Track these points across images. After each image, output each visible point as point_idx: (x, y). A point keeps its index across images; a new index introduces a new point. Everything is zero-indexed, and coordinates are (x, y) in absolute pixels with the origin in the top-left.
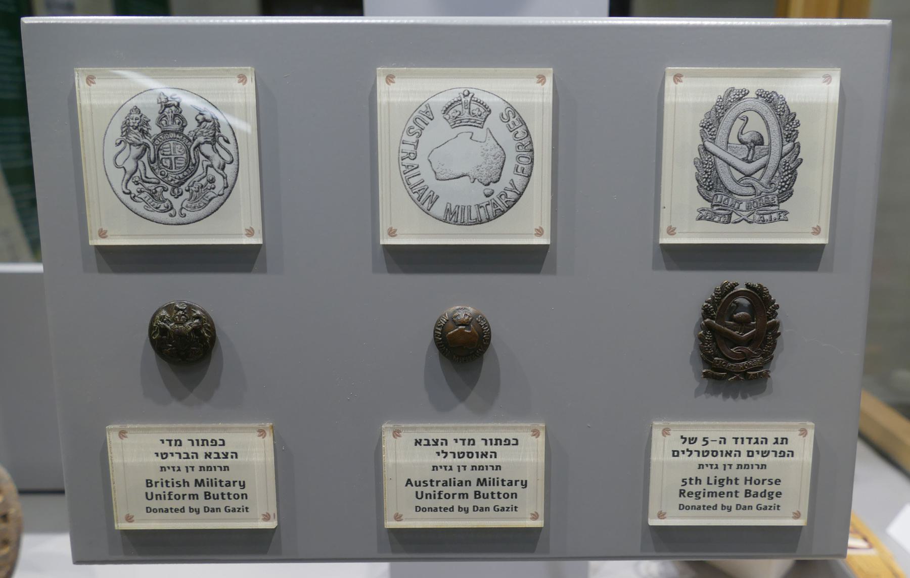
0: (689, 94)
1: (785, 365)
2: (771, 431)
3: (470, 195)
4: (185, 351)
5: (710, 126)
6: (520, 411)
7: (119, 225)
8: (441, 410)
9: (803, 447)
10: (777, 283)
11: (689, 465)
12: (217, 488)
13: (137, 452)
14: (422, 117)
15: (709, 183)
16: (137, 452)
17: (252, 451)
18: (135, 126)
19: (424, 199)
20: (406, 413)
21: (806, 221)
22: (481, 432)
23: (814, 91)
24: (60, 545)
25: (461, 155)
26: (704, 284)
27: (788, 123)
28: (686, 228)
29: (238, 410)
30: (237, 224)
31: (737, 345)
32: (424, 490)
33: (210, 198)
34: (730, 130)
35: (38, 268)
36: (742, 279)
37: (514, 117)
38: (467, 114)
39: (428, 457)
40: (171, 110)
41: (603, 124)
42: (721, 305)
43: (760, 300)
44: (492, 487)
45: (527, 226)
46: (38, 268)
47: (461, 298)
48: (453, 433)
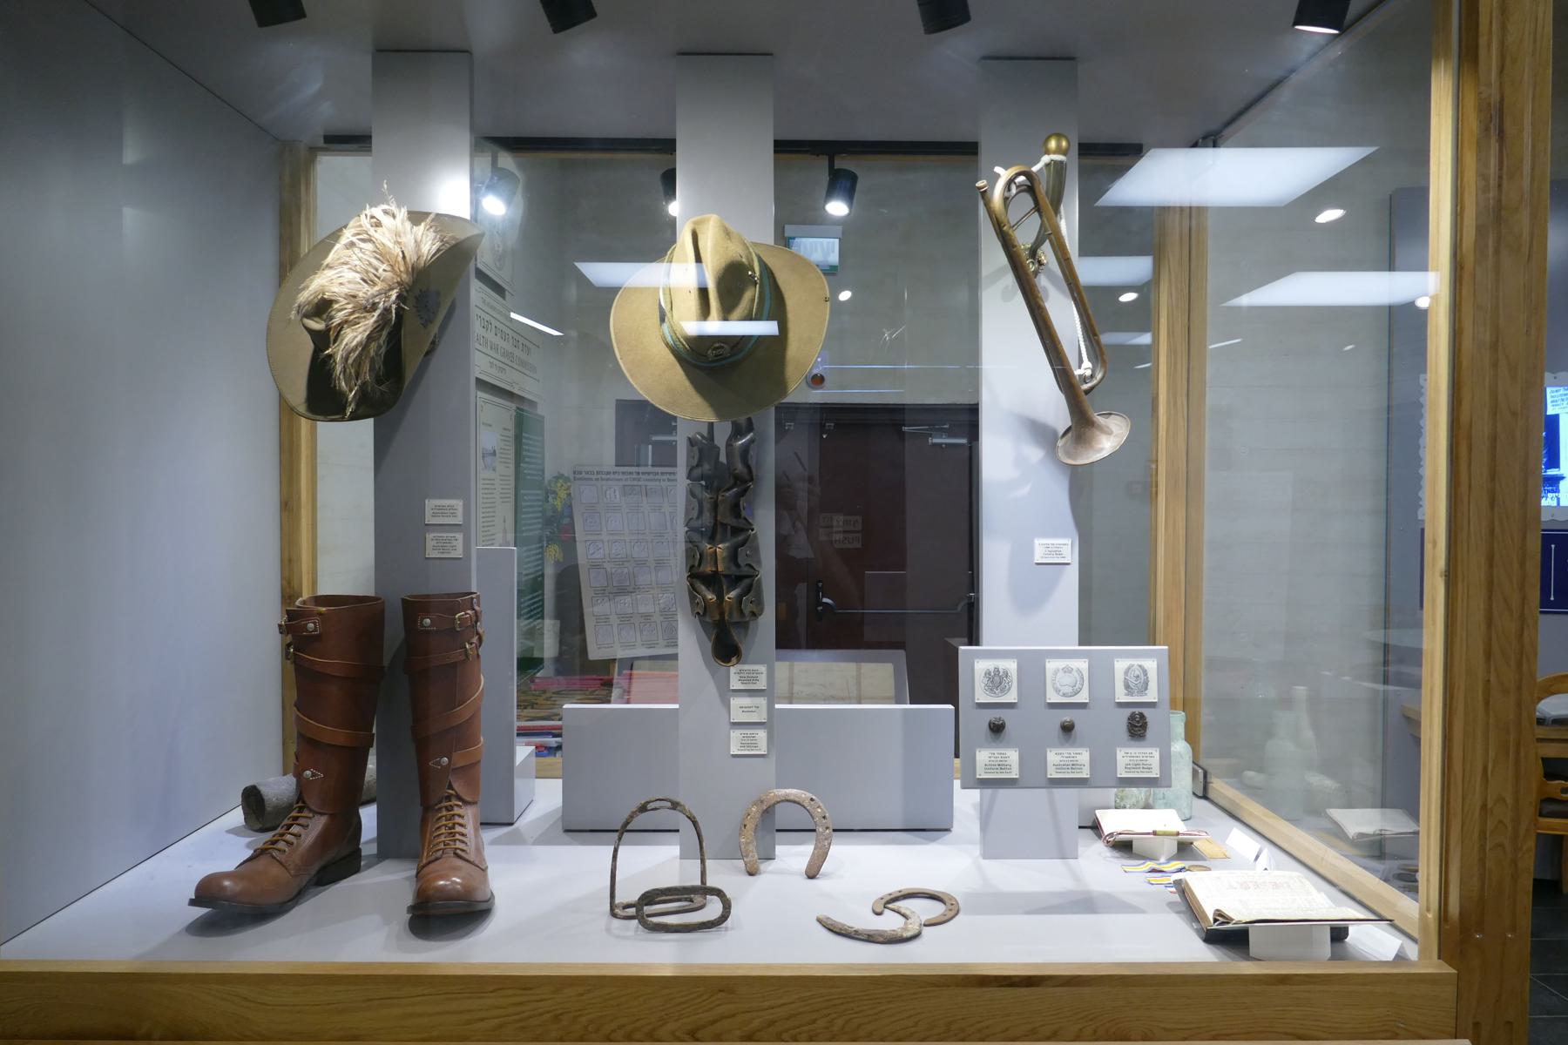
0: (1120, 665)
1: (1150, 733)
2: (1148, 750)
3: (1069, 690)
4: (997, 729)
5: (1126, 673)
6: (1082, 746)
7: (982, 697)
8: (1062, 745)
9: (1156, 753)
10: (1146, 712)
11: (1127, 760)
12: (1003, 766)
13: (983, 756)
14: (1056, 672)
15: (1127, 686)
16: (983, 756)
17: (1013, 756)
18: (988, 673)
19: (1057, 691)
20: (1053, 746)
21: (1151, 696)
22: (1072, 751)
23: (1151, 665)
24: (1548, 501)
25: (1066, 680)
26: (1128, 712)
27: (1145, 672)
28: (1121, 696)
29: (1009, 745)
30: (1011, 697)
31: (1137, 728)
32: (1058, 767)
33: (1004, 691)
34: (1131, 674)
35: (676, 706)
36: (1137, 710)
37: (1079, 671)
38: (1068, 670)
39: (1059, 758)
40: (997, 670)
41: (1100, 675)
42: (1132, 717)
43: (1142, 716)
44: (1075, 766)
45: (1083, 697)
46: (676, 706)
47: (1066, 716)
48: (1065, 751)
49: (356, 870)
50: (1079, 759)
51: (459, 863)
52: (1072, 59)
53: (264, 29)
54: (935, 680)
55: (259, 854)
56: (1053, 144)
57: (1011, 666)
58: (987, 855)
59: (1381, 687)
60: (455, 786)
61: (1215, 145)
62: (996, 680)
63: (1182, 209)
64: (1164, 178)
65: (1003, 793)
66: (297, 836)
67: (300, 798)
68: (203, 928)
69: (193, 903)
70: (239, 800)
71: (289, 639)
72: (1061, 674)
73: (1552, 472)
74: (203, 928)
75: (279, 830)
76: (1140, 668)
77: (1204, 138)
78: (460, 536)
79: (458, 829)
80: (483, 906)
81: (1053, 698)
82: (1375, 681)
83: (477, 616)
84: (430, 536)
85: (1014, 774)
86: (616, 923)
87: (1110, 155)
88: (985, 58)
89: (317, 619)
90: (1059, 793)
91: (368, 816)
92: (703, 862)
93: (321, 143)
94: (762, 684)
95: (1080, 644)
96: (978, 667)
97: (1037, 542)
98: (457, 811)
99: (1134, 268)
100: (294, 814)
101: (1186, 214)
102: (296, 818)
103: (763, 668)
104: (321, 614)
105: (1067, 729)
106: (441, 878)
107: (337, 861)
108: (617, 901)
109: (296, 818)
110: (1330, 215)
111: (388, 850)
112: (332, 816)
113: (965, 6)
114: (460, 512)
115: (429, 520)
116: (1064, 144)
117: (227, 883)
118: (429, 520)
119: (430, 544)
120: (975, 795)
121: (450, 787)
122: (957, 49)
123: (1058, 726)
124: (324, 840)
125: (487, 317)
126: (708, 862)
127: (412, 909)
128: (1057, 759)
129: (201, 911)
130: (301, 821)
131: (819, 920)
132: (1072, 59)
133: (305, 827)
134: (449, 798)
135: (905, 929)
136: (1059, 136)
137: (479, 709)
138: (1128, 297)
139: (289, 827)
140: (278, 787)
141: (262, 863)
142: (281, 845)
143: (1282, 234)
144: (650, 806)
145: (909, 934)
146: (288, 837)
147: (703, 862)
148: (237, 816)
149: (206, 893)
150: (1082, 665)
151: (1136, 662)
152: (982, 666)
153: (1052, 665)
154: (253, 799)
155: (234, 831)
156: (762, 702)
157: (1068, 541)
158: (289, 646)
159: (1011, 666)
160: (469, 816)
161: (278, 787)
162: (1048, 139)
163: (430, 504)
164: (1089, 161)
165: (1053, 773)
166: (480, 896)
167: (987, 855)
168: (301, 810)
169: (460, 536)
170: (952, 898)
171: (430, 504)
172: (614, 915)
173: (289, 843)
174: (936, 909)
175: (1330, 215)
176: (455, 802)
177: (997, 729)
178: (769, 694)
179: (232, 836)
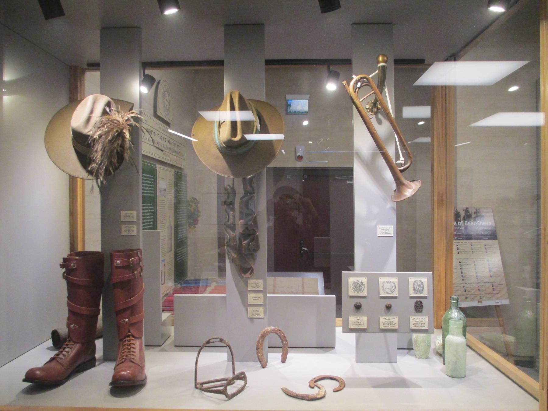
0: (412, 280)
2: (423, 317)
3: (389, 291)
4: (358, 307)
5: (414, 283)
7: (351, 293)
10: (422, 300)
12: (360, 323)
13: (352, 319)
14: (384, 282)
15: (414, 289)
16: (382, 319)
18: (354, 283)
19: (384, 291)
21: (425, 294)
22: (391, 317)
23: (425, 280)
25: (388, 286)
26: (415, 300)
27: (422, 283)
28: (412, 294)
30: (364, 293)
31: (419, 307)
32: (385, 324)
33: (361, 291)
36: (419, 300)
38: (389, 282)
39: (385, 320)
40: (358, 281)
41: (403, 285)
42: (417, 302)
43: (421, 302)
44: (391, 323)
45: (395, 294)
47: (388, 302)
49: (94, 366)
50: (393, 320)
51: (132, 364)
52: (391, 24)
53: (48, 20)
54: (333, 285)
55: (52, 359)
56: (380, 59)
57: (364, 280)
58: (359, 360)
59: (536, 290)
60: (131, 331)
61: (455, 60)
62: (358, 286)
63: (442, 87)
64: (443, 74)
65: (363, 335)
66: (68, 352)
67: (69, 337)
68: (30, 391)
69: (25, 380)
70: (50, 336)
71: (64, 270)
72: (386, 284)
73: (350, 182)
74: (30, 391)
75: (61, 350)
76: (421, 281)
77: (451, 56)
78: (135, 226)
79: (132, 349)
80: (140, 383)
81: (382, 294)
82: (533, 287)
83: (140, 260)
84: (123, 226)
85: (365, 327)
86: (197, 391)
87: (420, 64)
88: (354, 24)
89: (75, 262)
90: (389, 335)
91: (99, 344)
92: (233, 364)
93: (85, 66)
94: (261, 288)
95: (397, 271)
96: (350, 280)
97: (378, 227)
98: (132, 342)
99: (424, 112)
100: (67, 343)
101: (444, 88)
102: (67, 345)
103: (261, 281)
104: (76, 260)
105: (388, 307)
106: (122, 371)
107: (84, 362)
108: (198, 381)
109: (67, 345)
110: (513, 89)
111: (107, 358)
112: (82, 344)
113: (339, 2)
114: (135, 216)
115: (123, 219)
116: (385, 58)
117: (38, 372)
118: (123, 219)
119: (123, 230)
120: (352, 336)
121: (129, 332)
122: (334, 20)
123: (384, 306)
124: (78, 355)
125: (162, 135)
126: (236, 363)
127: (111, 384)
128: (384, 320)
129: (28, 384)
130: (69, 346)
131: (282, 390)
132: (391, 24)
133: (71, 348)
134: (129, 336)
135: (318, 394)
136: (384, 55)
137: (142, 298)
138: (421, 123)
139: (65, 348)
140: (63, 330)
141: (53, 364)
142: (61, 356)
143: (492, 97)
144: (211, 341)
145: (320, 396)
146: (64, 353)
147: (233, 364)
148: (50, 343)
149: (30, 377)
150: (395, 280)
151: (418, 279)
152: (351, 280)
153: (382, 280)
154: (55, 335)
155: (48, 349)
156: (261, 295)
157: (392, 227)
158: (64, 273)
159: (364, 280)
160: (137, 343)
161: (63, 330)
162: (378, 58)
163: (123, 213)
164: (400, 67)
165: (382, 327)
166: (139, 378)
167: (359, 360)
168: (69, 341)
169: (135, 226)
170: (341, 379)
171: (123, 213)
172: (196, 388)
173: (64, 355)
174: (335, 384)
175: (513, 89)
176: (131, 338)
177: (388, 307)
178: (264, 292)
179: (48, 351)
